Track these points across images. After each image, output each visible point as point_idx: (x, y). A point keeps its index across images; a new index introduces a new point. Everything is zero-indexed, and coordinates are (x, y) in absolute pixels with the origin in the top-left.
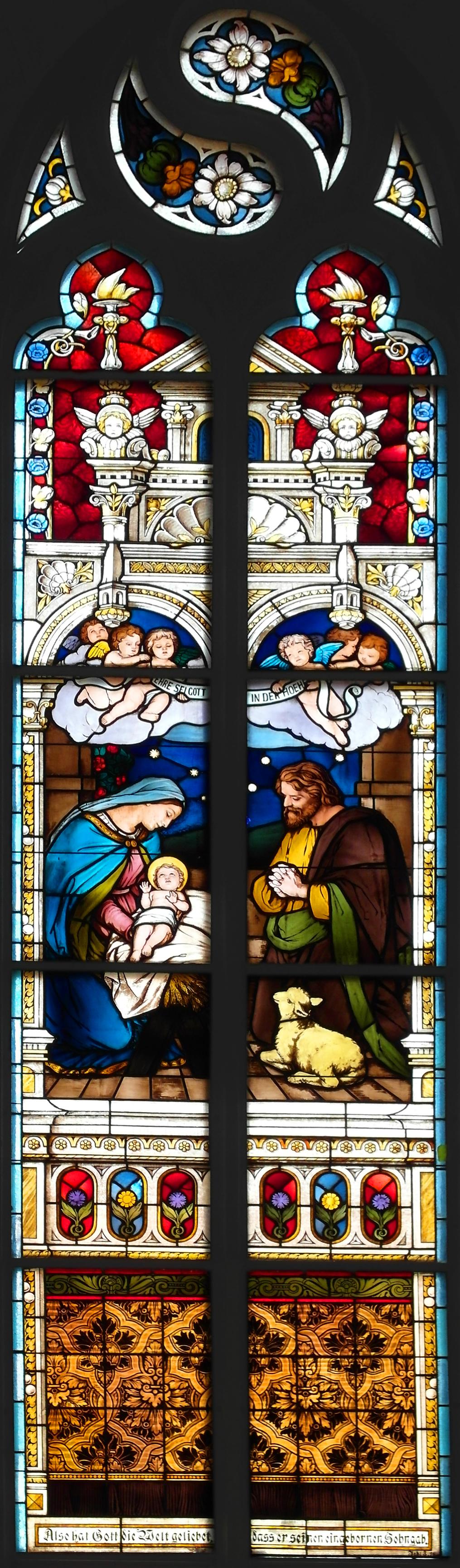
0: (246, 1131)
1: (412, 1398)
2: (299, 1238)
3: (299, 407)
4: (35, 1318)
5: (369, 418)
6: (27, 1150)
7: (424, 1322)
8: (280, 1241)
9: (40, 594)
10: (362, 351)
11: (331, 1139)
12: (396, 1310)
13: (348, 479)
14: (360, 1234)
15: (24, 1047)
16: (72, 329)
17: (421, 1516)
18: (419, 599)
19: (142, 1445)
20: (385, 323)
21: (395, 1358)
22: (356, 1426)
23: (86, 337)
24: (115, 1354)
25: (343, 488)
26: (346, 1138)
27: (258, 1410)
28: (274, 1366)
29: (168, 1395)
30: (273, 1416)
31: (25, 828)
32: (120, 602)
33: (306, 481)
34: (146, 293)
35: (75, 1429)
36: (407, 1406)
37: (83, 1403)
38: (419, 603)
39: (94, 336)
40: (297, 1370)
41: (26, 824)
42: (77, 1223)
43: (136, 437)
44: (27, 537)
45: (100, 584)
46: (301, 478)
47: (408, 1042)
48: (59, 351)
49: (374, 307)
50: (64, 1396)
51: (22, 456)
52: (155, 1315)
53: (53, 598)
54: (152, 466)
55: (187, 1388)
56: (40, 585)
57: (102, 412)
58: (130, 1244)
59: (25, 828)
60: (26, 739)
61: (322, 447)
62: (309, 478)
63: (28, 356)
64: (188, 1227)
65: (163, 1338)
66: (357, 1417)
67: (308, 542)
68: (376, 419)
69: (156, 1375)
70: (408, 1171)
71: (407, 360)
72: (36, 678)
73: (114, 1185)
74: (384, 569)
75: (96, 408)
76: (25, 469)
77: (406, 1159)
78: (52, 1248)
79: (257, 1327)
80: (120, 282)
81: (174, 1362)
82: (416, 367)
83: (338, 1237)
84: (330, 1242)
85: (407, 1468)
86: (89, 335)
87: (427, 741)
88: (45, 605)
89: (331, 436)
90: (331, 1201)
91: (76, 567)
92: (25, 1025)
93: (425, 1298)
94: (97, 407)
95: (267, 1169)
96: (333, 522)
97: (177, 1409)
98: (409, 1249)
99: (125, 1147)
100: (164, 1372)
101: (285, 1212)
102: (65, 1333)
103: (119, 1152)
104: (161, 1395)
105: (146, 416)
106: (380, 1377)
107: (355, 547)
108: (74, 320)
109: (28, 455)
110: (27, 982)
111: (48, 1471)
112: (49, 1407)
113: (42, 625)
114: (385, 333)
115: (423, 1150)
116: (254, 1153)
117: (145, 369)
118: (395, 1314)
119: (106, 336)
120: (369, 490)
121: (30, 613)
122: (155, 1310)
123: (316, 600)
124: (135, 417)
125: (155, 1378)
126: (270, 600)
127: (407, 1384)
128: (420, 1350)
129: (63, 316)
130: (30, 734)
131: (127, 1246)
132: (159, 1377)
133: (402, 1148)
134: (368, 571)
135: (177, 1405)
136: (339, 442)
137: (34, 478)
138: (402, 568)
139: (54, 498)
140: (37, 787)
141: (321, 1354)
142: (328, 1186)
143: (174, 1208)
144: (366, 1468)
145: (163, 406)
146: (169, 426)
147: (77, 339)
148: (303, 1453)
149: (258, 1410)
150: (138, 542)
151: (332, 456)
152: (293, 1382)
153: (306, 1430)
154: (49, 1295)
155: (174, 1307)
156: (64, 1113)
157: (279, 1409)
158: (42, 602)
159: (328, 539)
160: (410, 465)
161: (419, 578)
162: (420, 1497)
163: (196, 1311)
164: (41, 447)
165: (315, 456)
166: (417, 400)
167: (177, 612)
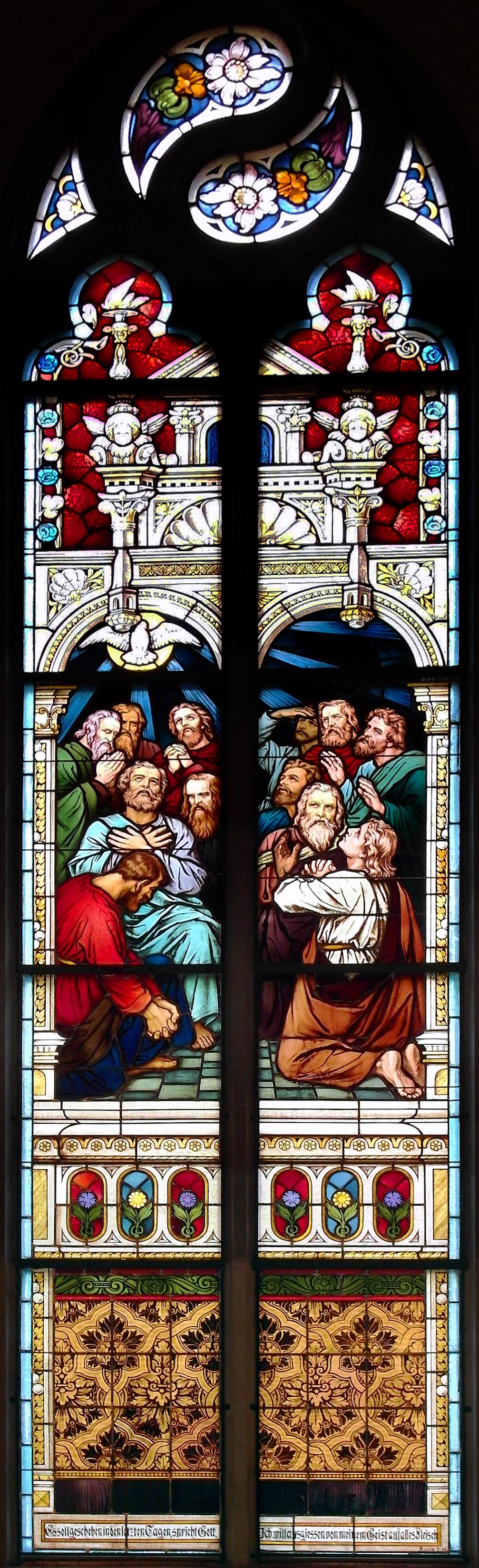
1: (423, 1395)
2: (105, 1238)
3: (309, 409)
4: (44, 1318)
5: (379, 419)
6: (37, 1153)
7: (436, 1319)
8: (291, 1240)
9: (51, 603)
10: (374, 351)
11: (345, 1138)
12: (154, 1306)
13: (358, 479)
14: (166, 1233)
15: (35, 1050)
16: (81, 339)
17: (430, 1511)
18: (430, 597)
19: (404, 1444)
20: (397, 322)
21: (406, 1357)
22: (367, 1423)
23: (96, 348)
24: (123, 1354)
25: (353, 489)
26: (359, 1136)
27: (269, 1408)
28: (132, 1362)
29: (174, 1394)
30: (283, 1412)
32: (130, 607)
33: (317, 482)
34: (156, 301)
35: (82, 1428)
36: (417, 1403)
37: (90, 1402)
38: (430, 601)
39: (103, 345)
40: (308, 1368)
41: (38, 831)
42: (188, 1224)
43: (144, 444)
44: (37, 547)
45: (111, 589)
46: (312, 480)
47: (56, 1040)
48: (68, 362)
49: (385, 306)
50: (326, 1396)
51: (33, 467)
52: (163, 1314)
54: (160, 470)
55: (93, 1387)
56: (51, 594)
57: (110, 421)
58: (346, 1244)
59: (36, 834)
61: (331, 448)
62: (320, 479)
63: (37, 368)
64: (199, 1226)
65: (171, 1337)
66: (367, 1415)
67: (318, 543)
68: (386, 419)
69: (163, 1373)
70: (421, 1168)
71: (418, 358)
73: (329, 1187)
74: (394, 568)
75: (104, 417)
76: (36, 479)
77: (419, 1156)
78: (63, 1249)
79: (267, 1325)
80: (130, 291)
81: (182, 1362)
82: (427, 366)
83: (350, 1235)
84: (342, 1240)
85: (418, 1465)
86: (99, 346)
87: (442, 737)
88: (57, 611)
89: (342, 438)
90: (137, 1199)
91: (86, 574)
92: (36, 1029)
93: (437, 1294)
94: (142, 416)
95: (278, 1168)
96: (344, 523)
97: (83, 1408)
98: (422, 1247)
99: (136, 1147)
100: (171, 1371)
101: (296, 1211)
102: (74, 1333)
103: (130, 1153)
104: (168, 1394)
105: (156, 422)
106: (290, 1374)
107: (368, 547)
108: (83, 331)
109: (38, 466)
110: (38, 986)
111: (55, 1469)
112: (57, 1407)
113: (54, 632)
114: (395, 331)
115: (408, 1147)
116: (268, 1151)
117: (153, 377)
118: (152, 1311)
119: (115, 345)
120: (380, 489)
121: (41, 621)
122: (162, 1309)
123: (334, 602)
124: (143, 424)
125: (162, 1377)
126: (280, 602)
127: (417, 1382)
128: (431, 1347)
129: (73, 327)
130: (42, 741)
131: (342, 1246)
132: (166, 1376)
133: (416, 1145)
134: (378, 570)
135: (83, 1404)
136: (349, 443)
137: (44, 487)
138: (413, 567)
139: (65, 507)
141: (78, 1351)
142: (340, 1185)
143: (184, 1208)
144: (375, 1465)
145: (171, 412)
146: (177, 431)
147: (87, 350)
148: (313, 1450)
149: (269, 1408)
150: (148, 547)
151: (342, 457)
152: (304, 1380)
153: (316, 1428)
154: (59, 1296)
155: (335, 1307)
157: (136, 1407)
158: (53, 610)
159: (338, 539)
160: (421, 463)
161: (431, 575)
162: (429, 1492)
163: (206, 1311)
164: (51, 457)
165: (325, 458)
166: (427, 400)
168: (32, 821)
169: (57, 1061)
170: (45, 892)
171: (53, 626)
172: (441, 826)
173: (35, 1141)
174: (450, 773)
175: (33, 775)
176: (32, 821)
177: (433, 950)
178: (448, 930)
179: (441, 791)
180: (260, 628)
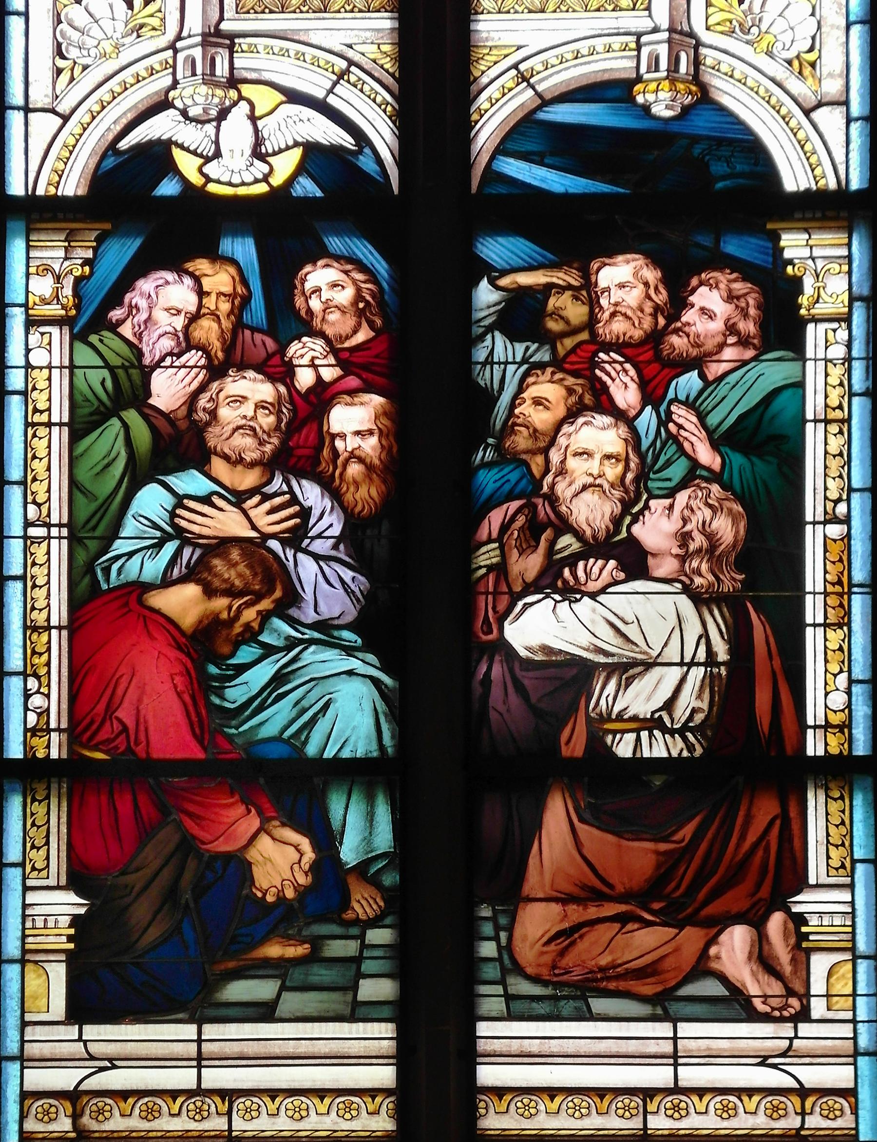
0: (399, 1030)
9: (61, 63)
11: (648, 1094)
15: (29, 924)
18: (812, 57)
26: (677, 1090)
31: (31, 508)
38: (813, 65)
41: (34, 502)
45: (179, 38)
53: (85, 68)
56: (59, 45)
59: (31, 508)
60: (34, 339)
72: (54, 219)
77: (798, 1130)
87: (835, 325)
88: (72, 79)
99: (229, 1113)
113: (66, 118)
121: (40, 96)
126: (515, 66)
130: (42, 329)
140: (55, 430)
156: (770, 1061)
158: (65, 77)
161: (813, 14)
167: (329, 85)
168: (23, 483)
169: (71, 946)
170: (48, 620)
171: (64, 107)
172: (833, 495)
173: (27, 1103)
174: (851, 395)
175: (24, 393)
176: (23, 483)
177: (820, 733)
178: (849, 693)
179: (834, 428)
180: (475, 117)
